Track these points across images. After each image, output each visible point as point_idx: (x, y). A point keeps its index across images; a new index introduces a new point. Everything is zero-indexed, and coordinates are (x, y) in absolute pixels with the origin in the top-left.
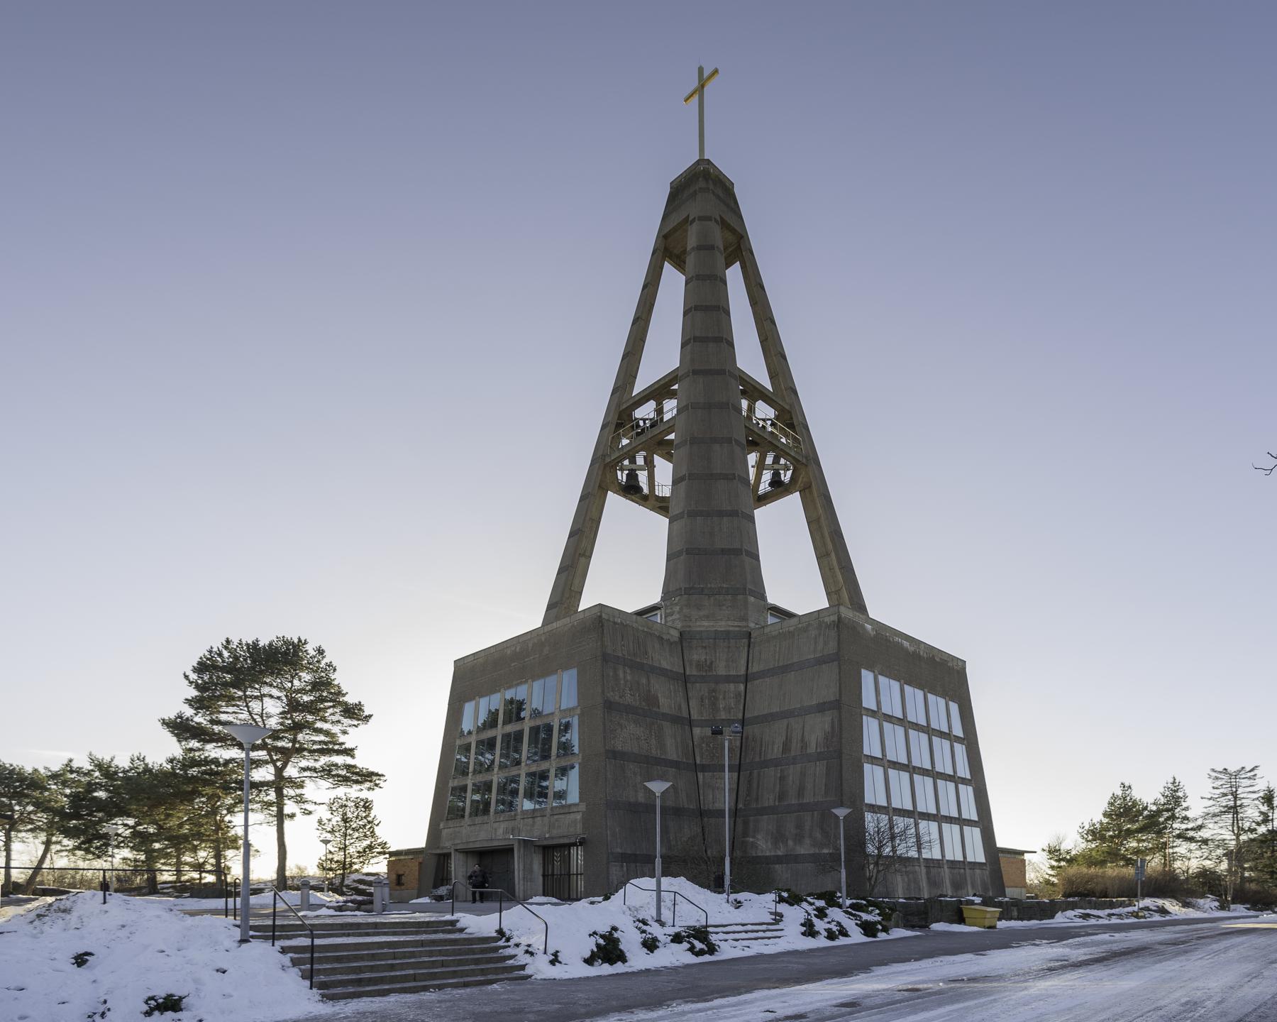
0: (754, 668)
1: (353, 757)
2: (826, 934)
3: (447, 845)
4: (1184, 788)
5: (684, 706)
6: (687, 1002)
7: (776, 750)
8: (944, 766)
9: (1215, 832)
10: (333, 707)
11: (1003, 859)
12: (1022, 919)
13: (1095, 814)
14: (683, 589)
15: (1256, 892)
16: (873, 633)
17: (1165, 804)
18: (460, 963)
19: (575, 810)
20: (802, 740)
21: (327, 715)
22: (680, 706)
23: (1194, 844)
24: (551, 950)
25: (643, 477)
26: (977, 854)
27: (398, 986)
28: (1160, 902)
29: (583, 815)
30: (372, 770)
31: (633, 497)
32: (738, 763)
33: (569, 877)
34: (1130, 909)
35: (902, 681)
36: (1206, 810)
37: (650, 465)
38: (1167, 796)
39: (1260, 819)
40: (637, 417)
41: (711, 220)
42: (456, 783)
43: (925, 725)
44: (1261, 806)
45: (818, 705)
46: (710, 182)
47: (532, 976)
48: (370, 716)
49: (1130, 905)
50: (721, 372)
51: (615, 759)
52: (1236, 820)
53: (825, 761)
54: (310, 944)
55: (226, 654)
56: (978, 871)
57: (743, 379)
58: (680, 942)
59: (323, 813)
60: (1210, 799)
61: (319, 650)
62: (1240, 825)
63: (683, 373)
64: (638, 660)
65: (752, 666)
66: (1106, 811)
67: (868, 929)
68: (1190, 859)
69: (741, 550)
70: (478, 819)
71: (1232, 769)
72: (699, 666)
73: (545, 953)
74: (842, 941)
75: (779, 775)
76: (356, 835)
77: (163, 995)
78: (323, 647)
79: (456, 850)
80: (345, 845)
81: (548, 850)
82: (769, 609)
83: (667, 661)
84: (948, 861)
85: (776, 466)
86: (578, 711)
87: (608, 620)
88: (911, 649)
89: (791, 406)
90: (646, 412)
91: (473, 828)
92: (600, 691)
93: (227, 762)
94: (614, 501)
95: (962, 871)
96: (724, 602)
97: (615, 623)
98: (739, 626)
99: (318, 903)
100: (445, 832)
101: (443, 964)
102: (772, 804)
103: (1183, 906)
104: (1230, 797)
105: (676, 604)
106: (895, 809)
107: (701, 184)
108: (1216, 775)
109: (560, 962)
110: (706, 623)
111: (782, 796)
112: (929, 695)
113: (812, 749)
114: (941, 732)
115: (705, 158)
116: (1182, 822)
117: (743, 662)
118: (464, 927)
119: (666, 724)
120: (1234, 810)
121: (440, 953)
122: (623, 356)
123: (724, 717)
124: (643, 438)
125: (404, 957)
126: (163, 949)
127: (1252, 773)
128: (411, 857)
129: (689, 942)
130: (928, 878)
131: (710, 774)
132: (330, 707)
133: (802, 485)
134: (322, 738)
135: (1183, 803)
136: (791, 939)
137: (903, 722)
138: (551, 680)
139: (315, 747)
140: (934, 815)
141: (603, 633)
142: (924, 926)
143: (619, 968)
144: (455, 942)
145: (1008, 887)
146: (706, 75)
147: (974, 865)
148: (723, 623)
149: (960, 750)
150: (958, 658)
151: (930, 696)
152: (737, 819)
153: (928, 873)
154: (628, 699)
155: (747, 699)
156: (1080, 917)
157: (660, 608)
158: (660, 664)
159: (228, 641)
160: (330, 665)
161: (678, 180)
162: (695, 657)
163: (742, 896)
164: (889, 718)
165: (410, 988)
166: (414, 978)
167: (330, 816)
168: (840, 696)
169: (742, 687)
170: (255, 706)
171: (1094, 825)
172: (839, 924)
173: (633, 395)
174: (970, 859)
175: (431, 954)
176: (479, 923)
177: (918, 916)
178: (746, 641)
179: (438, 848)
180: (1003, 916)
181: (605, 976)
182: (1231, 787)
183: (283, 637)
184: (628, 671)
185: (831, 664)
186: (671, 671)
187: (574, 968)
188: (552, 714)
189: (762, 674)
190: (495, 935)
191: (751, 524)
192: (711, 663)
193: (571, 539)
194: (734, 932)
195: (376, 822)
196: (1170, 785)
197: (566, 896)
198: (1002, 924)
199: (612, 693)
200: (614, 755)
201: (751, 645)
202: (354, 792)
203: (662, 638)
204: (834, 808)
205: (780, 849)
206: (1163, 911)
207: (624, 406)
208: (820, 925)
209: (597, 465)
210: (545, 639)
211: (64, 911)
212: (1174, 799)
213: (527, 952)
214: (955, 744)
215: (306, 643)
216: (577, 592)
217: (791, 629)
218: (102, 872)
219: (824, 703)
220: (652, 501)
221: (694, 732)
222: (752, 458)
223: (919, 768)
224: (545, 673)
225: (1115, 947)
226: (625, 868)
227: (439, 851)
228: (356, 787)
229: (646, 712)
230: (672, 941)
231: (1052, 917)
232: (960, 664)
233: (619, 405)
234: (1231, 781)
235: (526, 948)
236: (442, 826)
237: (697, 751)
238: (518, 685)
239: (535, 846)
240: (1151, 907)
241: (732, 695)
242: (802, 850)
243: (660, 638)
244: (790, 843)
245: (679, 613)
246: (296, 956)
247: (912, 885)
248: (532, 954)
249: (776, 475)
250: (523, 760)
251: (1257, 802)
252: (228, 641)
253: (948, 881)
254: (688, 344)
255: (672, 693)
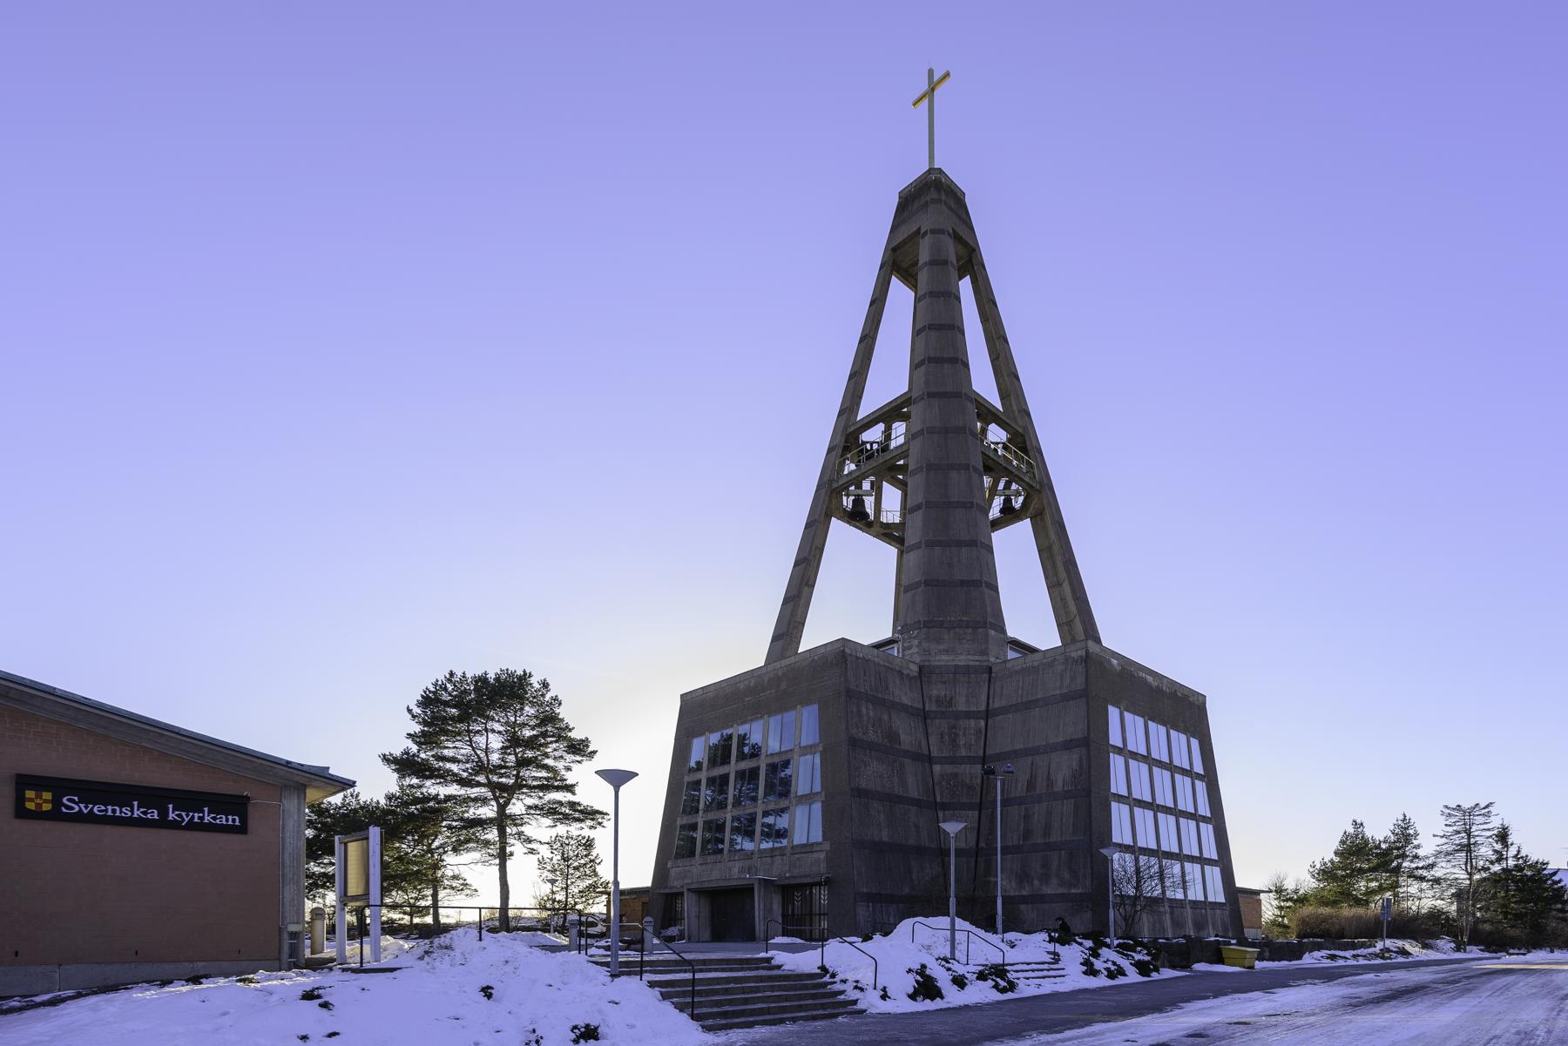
0: (997, 704)
1: (574, 793)
2: (1106, 973)
3: (675, 884)
4: (1415, 825)
5: (924, 743)
6: (1041, 1033)
7: (1020, 789)
8: (1186, 804)
9: (1448, 871)
10: (556, 742)
11: (1242, 899)
12: (1273, 960)
13: (1326, 851)
14: (922, 622)
15: (1490, 933)
16: (1119, 668)
17: (1395, 842)
18: (800, 997)
19: (818, 849)
20: (1048, 778)
21: (549, 750)
22: (920, 742)
23: (1425, 884)
24: (880, 986)
25: (869, 503)
26: (1217, 895)
27: (760, 1018)
28: (1400, 943)
29: (827, 854)
30: (597, 809)
31: (857, 524)
32: (979, 801)
33: (811, 919)
34: (1371, 950)
35: (1146, 717)
36: (1438, 848)
37: (877, 490)
38: (1397, 834)
39: (1494, 858)
40: (864, 440)
41: (944, 233)
42: (685, 820)
43: (1168, 762)
44: (1495, 845)
45: (1064, 742)
46: (943, 193)
47: (866, 1010)
48: (595, 752)
49: (1370, 946)
50: (958, 395)
51: (859, 797)
52: (1469, 859)
53: (1073, 800)
54: (692, 977)
55: (450, 687)
56: (1218, 911)
57: (979, 403)
58: (985, 980)
59: (545, 851)
60: (1442, 837)
61: (544, 684)
62: (1474, 863)
63: (917, 395)
64: (880, 696)
65: (993, 701)
66: (1338, 850)
67: (1143, 968)
68: (1421, 899)
69: (980, 581)
70: (710, 859)
71: (1466, 805)
72: (939, 701)
73: (875, 989)
74: (1121, 980)
75: (1023, 814)
76: (578, 874)
77: (583, 1025)
78: (548, 681)
79: (689, 890)
80: (567, 884)
81: (787, 890)
82: (1009, 642)
83: (907, 697)
84: (1189, 901)
85: (1007, 492)
86: (821, 748)
87: (851, 655)
88: (1155, 684)
89: (1024, 428)
90: (873, 435)
91: (704, 867)
92: (844, 727)
93: (448, 798)
94: (837, 527)
95: (1203, 911)
96: (964, 636)
97: (858, 658)
98: (980, 661)
99: (549, 944)
100: (673, 872)
101: (787, 998)
102: (1016, 843)
103: (1423, 948)
104: (1464, 835)
105: (915, 638)
106: (1141, 849)
107: (933, 195)
108: (1449, 811)
109: (889, 998)
110: (945, 657)
111: (1027, 834)
112: (1172, 732)
113: (1059, 787)
114: (1183, 769)
115: (936, 167)
116: (1412, 861)
117: (984, 697)
118: (780, 964)
119: (907, 762)
120: (1468, 848)
121: (780, 988)
122: (850, 375)
123: (964, 754)
124: (873, 463)
125: (751, 992)
126: (550, 983)
127: (1486, 810)
128: (633, 897)
129: (992, 980)
130: (1172, 919)
131: (951, 812)
132: (551, 742)
133: (1034, 512)
134: (544, 774)
135: (1414, 841)
136: (1073, 978)
137: (1147, 759)
138: (789, 716)
139: (535, 783)
140: (1177, 854)
141: (846, 668)
142: (1186, 966)
143: (937, 1004)
144: (770, 978)
145: (1248, 928)
146: (937, 77)
147: (1215, 905)
148: (963, 657)
149: (1201, 786)
150: (1199, 693)
151: (1172, 732)
152: (979, 859)
153: (1172, 913)
154: (872, 736)
155: (988, 735)
156: (1328, 958)
157: (897, 642)
158: (900, 699)
159: (452, 674)
160: (555, 699)
161: (907, 190)
162: (935, 692)
163: (1011, 936)
164: (1134, 756)
165: (770, 1020)
166: (768, 1011)
167: (550, 856)
168: (1089, 734)
169: (983, 723)
170: (481, 740)
171: (1325, 864)
172: (1114, 963)
173: (858, 419)
174: (1211, 899)
175: (772, 989)
176: (804, 961)
177: (1182, 956)
178: (986, 675)
179: (666, 887)
180: (1261, 958)
181: (932, 1011)
182: (1464, 824)
183: (507, 670)
184: (871, 707)
185: (1078, 700)
186: (911, 707)
187: (901, 1004)
188: (791, 750)
189: (1004, 710)
190: (819, 971)
191: (990, 555)
192: (951, 699)
193: (798, 568)
194: (1023, 971)
195: (598, 861)
196: (1400, 822)
197: (808, 936)
198: (1259, 965)
199: (855, 730)
200: (859, 793)
201: (992, 680)
202: (574, 829)
203: (903, 674)
204: (1102, 848)
205: (1025, 889)
206: (1404, 952)
207: (852, 429)
208: (1098, 964)
209: (824, 491)
210: (783, 674)
211: (446, 948)
212: (1405, 835)
213: (856, 987)
214: (1196, 781)
215: (530, 676)
216: (800, 623)
217: (1036, 664)
218: (478, 910)
219: (1071, 740)
220: (876, 528)
221: (934, 770)
222: (987, 481)
223: (1162, 806)
224: (781, 709)
225: (1396, 986)
226: (871, 909)
227: (667, 891)
228: (578, 825)
229: (888, 749)
230: (978, 978)
231: (1300, 958)
232: (1201, 698)
233: (846, 428)
234: (1465, 818)
235: (855, 984)
236: (669, 865)
237: (936, 788)
238: (752, 720)
239: (775, 886)
240: (1391, 948)
241: (973, 732)
242: (1048, 890)
243: (900, 673)
244: (1036, 883)
245: (917, 646)
246: (664, 990)
247: (1157, 925)
248: (862, 989)
249: (1007, 501)
250: (759, 798)
251: (1490, 840)
252: (452, 674)
253: (1190, 921)
254: (922, 365)
255: (913, 730)
